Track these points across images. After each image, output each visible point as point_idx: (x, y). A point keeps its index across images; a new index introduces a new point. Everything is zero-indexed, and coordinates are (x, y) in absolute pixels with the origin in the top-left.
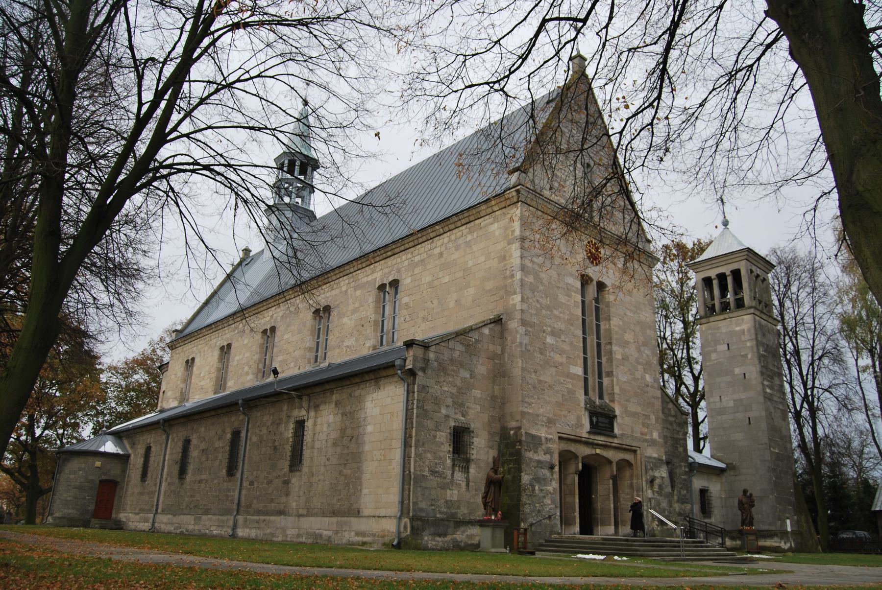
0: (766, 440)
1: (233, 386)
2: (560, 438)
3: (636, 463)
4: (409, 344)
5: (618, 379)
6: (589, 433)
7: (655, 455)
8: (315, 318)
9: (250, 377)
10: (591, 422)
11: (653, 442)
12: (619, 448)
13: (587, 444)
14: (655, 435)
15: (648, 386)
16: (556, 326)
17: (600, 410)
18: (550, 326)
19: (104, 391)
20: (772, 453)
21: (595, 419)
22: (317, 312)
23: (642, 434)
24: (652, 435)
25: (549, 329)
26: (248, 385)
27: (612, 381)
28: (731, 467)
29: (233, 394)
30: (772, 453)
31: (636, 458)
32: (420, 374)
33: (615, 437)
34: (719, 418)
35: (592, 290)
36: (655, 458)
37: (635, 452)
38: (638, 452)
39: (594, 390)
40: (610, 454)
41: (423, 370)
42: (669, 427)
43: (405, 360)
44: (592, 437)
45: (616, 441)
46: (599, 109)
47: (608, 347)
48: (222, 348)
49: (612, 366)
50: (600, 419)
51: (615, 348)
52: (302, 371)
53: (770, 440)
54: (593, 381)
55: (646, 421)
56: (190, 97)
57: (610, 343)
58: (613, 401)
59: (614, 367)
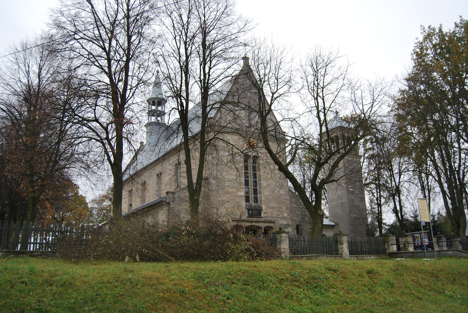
0: (348, 212)
1: (134, 207)
2: (233, 221)
3: (275, 227)
4: (167, 193)
5: (264, 195)
6: (248, 217)
7: (286, 223)
8: (158, 178)
9: (139, 203)
10: (248, 213)
11: (284, 218)
12: (264, 222)
13: (248, 221)
14: (285, 215)
15: (281, 195)
16: (230, 178)
17: (254, 208)
18: (227, 178)
19: (91, 212)
20: (351, 217)
21: (250, 212)
22: (158, 175)
23: (277, 215)
24: (283, 215)
25: (227, 180)
26: (139, 206)
27: (261, 195)
28: (337, 224)
29: (134, 210)
30: (351, 217)
31: (275, 225)
32: (172, 203)
33: (262, 218)
34: (332, 203)
35: (251, 161)
36: (285, 224)
37: (274, 222)
38: (276, 222)
39: (252, 200)
40: (261, 225)
41: (173, 202)
42: (300, 210)
43: (166, 199)
44: (249, 219)
45: (262, 219)
46: (256, 79)
47: (260, 182)
48: (129, 191)
49: (261, 189)
50: (253, 211)
51: (262, 182)
52: (155, 200)
53: (350, 211)
54: (252, 196)
55: (281, 210)
56: (165, 6)
57: (260, 180)
58: (261, 203)
59: (262, 190)
